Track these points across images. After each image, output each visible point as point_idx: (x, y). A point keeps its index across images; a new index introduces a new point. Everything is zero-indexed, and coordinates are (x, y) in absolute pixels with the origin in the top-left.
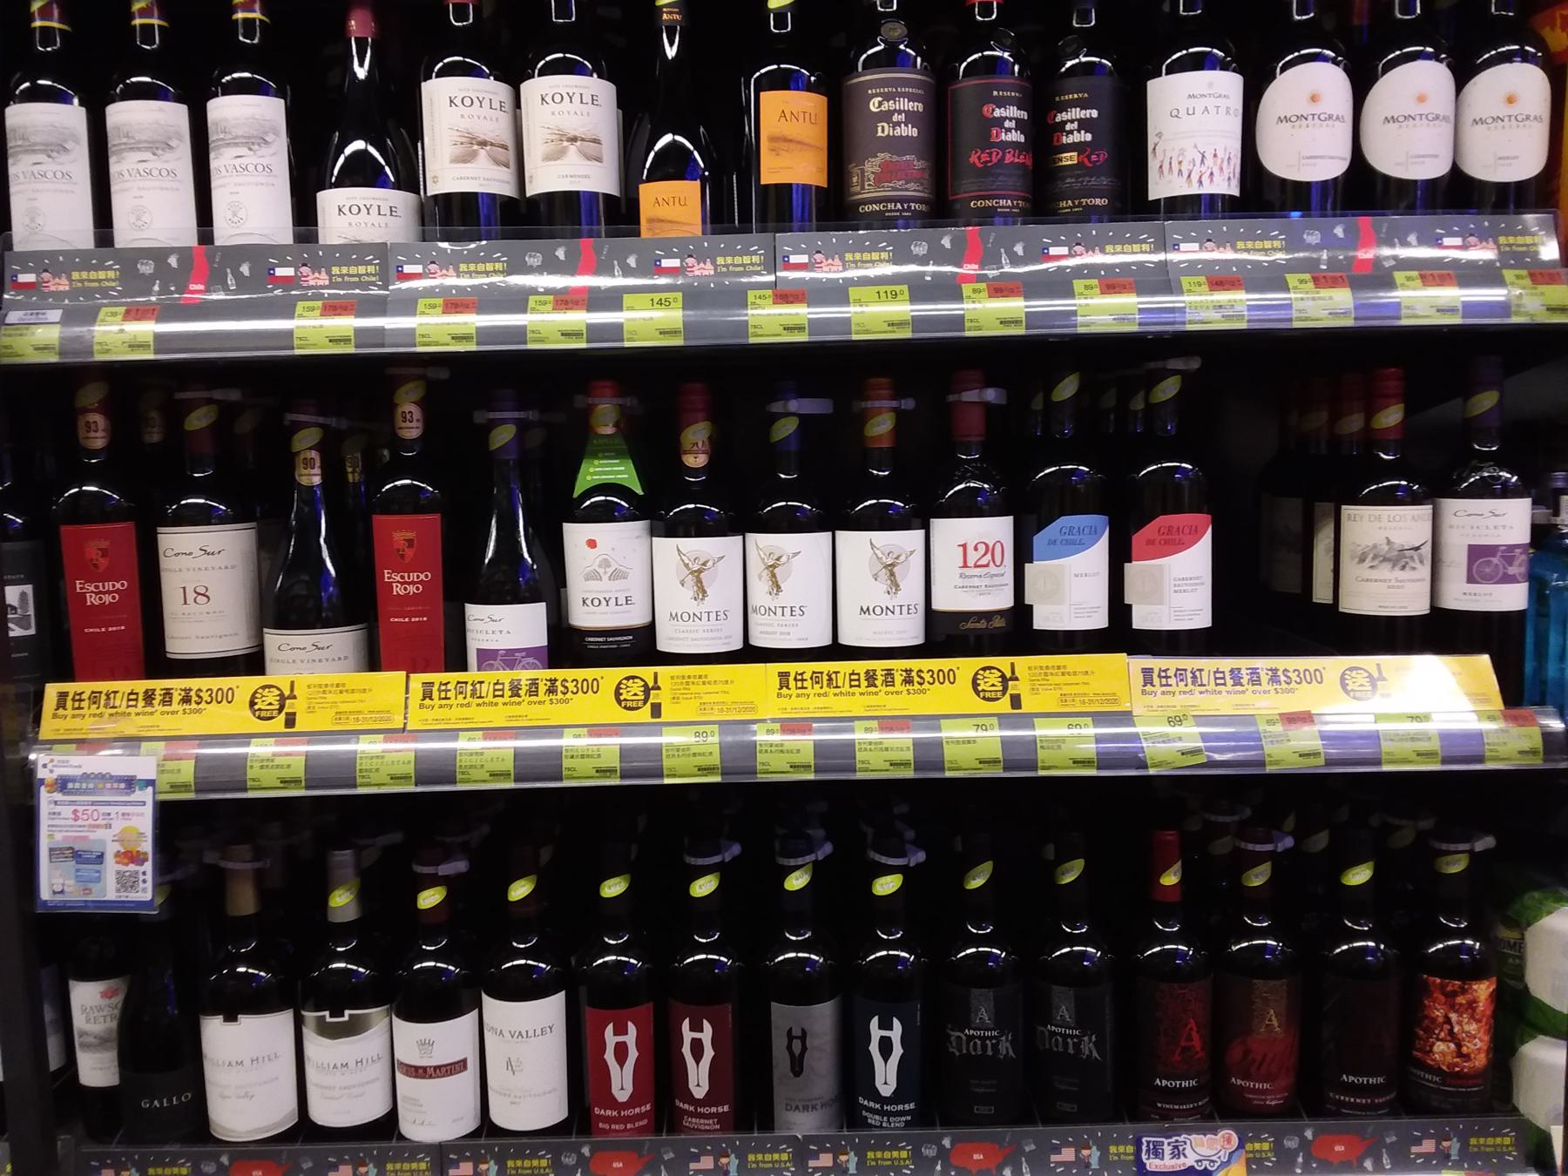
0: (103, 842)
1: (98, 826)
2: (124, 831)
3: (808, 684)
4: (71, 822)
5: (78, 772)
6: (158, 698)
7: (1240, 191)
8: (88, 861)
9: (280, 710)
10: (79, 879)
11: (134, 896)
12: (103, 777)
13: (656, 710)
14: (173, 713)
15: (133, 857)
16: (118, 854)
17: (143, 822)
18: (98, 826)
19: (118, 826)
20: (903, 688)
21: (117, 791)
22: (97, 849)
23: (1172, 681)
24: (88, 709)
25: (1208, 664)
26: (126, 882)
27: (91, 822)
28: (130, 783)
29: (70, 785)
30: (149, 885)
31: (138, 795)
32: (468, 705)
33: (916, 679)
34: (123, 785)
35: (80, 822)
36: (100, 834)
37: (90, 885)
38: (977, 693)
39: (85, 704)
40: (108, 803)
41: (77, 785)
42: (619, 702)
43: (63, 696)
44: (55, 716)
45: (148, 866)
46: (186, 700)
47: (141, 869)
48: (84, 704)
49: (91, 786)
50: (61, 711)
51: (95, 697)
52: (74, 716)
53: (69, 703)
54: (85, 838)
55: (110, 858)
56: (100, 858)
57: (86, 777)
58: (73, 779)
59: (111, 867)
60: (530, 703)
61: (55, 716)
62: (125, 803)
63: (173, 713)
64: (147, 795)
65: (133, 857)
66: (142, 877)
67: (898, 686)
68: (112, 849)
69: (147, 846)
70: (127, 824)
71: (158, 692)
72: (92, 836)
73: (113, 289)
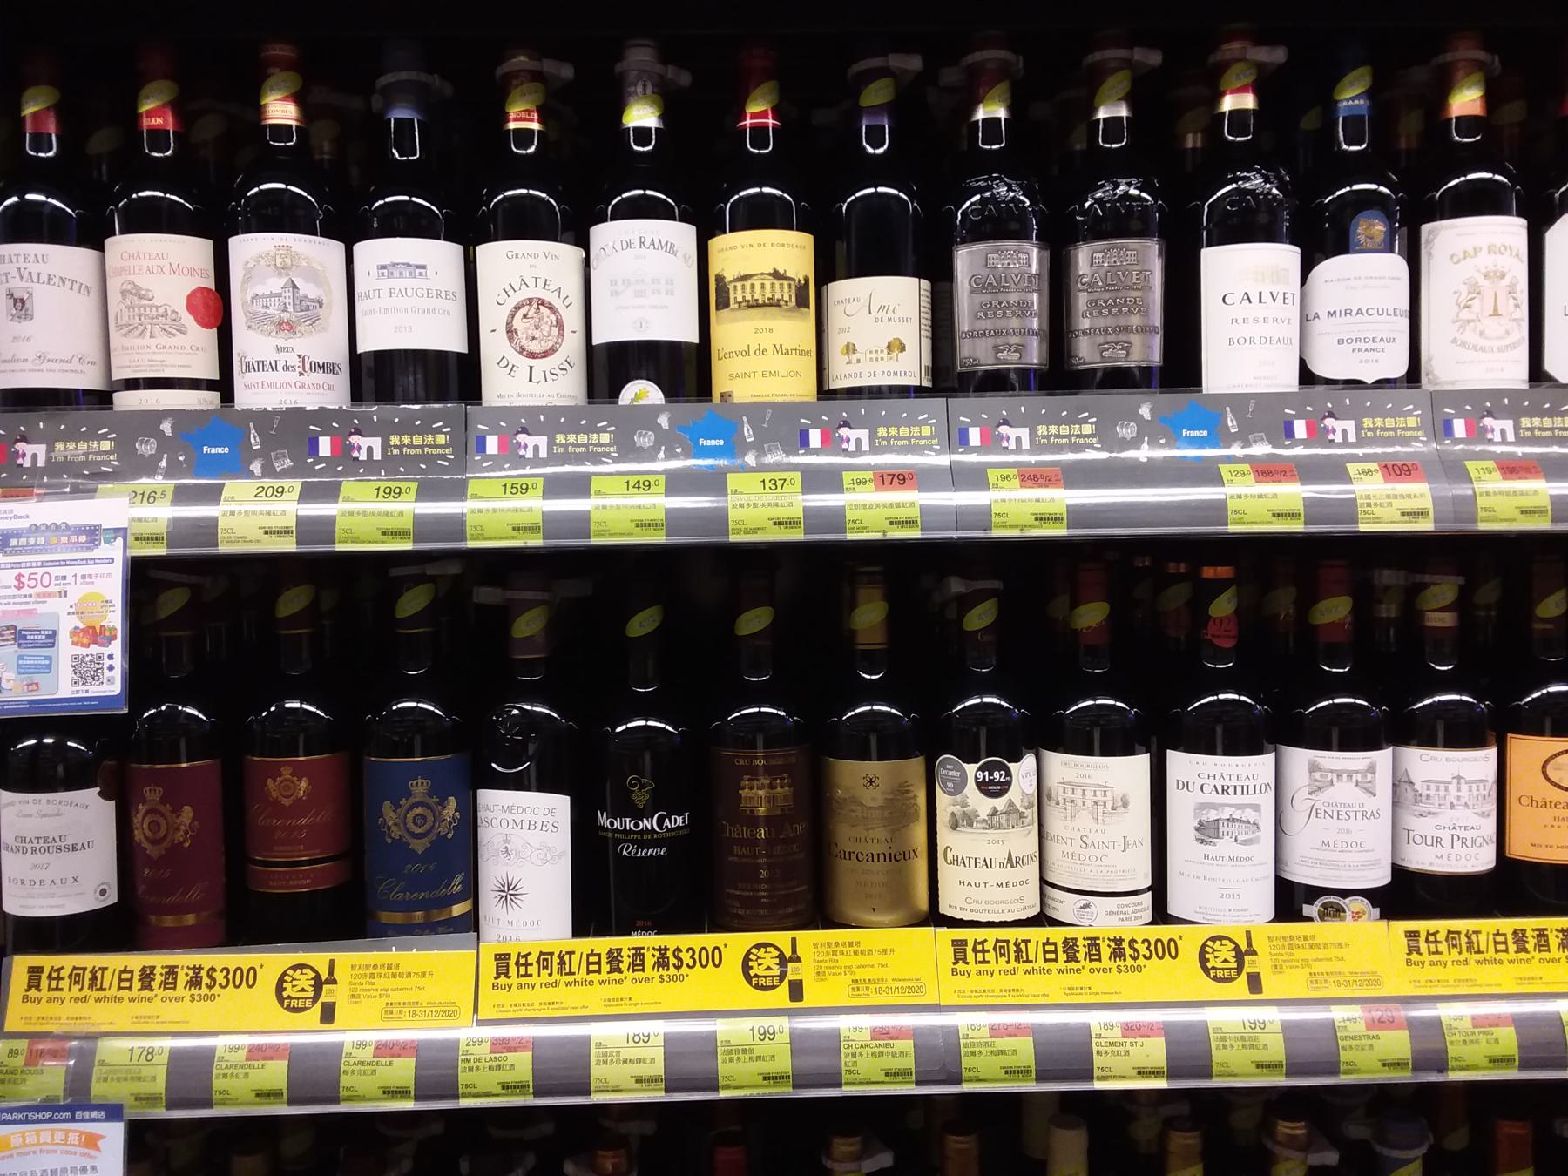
0: (55, 616)
1: (49, 595)
2: (83, 601)
3: (990, 956)
4: (16, 592)
5: (23, 524)
6: (158, 979)
7: (1400, 360)
8: (36, 645)
9: (315, 999)
10: (21, 670)
11: (95, 690)
12: (56, 528)
13: (796, 991)
14: (178, 999)
15: (95, 635)
16: (75, 632)
17: (111, 587)
18: (49, 595)
19: (76, 592)
20: (1113, 964)
21: (78, 547)
22: (47, 626)
23: (1443, 947)
24: (69, 991)
25: (1486, 927)
26: (86, 671)
27: (39, 589)
28: (93, 534)
29: (14, 542)
30: (117, 674)
31: (103, 551)
32: (555, 984)
33: (1129, 952)
34: (83, 538)
35: (23, 592)
36: (53, 605)
37: (37, 678)
38: (1206, 970)
39: (64, 984)
40: (65, 563)
41: (23, 541)
42: (748, 978)
43: (35, 972)
44: (25, 999)
45: (116, 647)
46: (195, 982)
47: (106, 651)
48: (63, 984)
49: (41, 541)
50: (33, 993)
51: (76, 976)
52: (50, 1000)
53: (44, 982)
54: (31, 612)
55: (64, 639)
56: (53, 636)
57: (35, 529)
58: (17, 534)
59: (66, 650)
60: (634, 981)
61: (25, 999)
62: (86, 562)
63: (178, 999)
64: (115, 552)
65: (95, 635)
66: (107, 663)
67: (1106, 961)
68: (67, 625)
69: (115, 619)
70: (88, 589)
71: (158, 971)
72: (41, 608)
73: (107, 463)
